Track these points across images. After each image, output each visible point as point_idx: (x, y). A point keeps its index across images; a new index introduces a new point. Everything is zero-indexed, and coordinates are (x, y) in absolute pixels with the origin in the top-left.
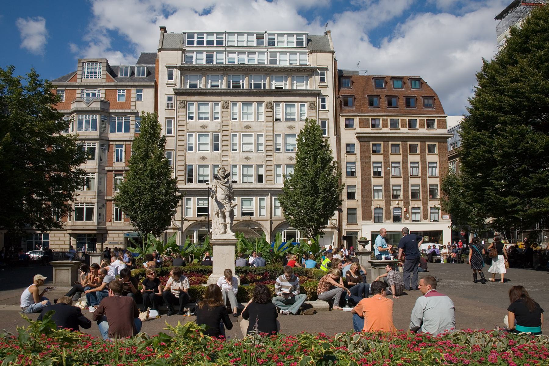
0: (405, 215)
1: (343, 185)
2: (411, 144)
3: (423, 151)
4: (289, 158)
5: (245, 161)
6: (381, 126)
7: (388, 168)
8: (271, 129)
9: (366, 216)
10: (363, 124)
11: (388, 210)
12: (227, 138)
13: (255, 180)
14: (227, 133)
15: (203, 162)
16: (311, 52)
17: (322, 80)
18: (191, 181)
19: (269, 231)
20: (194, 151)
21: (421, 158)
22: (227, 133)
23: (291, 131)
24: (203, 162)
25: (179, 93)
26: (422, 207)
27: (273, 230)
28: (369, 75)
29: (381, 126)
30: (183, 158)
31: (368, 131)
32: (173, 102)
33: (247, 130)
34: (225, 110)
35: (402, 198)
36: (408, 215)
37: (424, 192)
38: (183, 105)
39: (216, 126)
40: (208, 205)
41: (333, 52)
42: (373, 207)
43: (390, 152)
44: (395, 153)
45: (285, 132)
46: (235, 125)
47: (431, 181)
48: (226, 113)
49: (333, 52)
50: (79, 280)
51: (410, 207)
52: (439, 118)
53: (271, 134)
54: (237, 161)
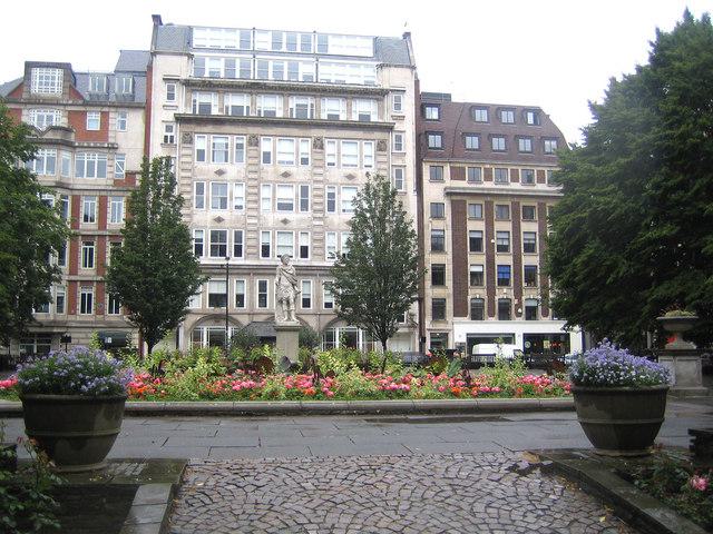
0: (516, 310)
8: (321, 178)
9: (460, 311)
11: (491, 301)
17: (398, 106)
25: (180, 119)
36: (520, 310)
37: (517, 273)
39: (239, 172)
42: (469, 297)
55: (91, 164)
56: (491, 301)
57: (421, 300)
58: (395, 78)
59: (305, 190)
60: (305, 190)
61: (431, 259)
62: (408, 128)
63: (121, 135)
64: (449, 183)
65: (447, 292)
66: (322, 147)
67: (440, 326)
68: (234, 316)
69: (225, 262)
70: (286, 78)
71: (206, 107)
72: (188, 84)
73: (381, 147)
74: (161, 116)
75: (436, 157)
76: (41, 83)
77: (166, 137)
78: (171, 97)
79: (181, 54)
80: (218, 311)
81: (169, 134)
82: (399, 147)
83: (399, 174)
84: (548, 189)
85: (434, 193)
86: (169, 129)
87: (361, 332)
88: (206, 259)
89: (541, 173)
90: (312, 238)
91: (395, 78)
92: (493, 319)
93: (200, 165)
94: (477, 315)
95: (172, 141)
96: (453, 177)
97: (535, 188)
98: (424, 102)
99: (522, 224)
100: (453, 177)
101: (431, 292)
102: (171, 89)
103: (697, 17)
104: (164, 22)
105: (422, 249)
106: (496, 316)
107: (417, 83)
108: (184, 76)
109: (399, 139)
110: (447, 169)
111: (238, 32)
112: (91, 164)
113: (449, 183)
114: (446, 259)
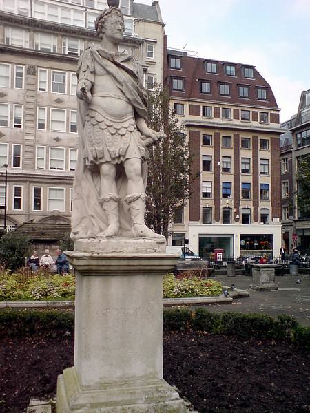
0: (235, 216)
2: (240, 139)
3: (255, 146)
4: (55, 139)
6: (251, 119)
7: (219, 163)
9: (194, 217)
10: (194, 111)
11: (217, 209)
16: (138, 21)
17: (150, 54)
18: (17, 163)
20: (45, 130)
21: (253, 154)
26: (252, 208)
27: (11, 216)
28: (200, 57)
29: (251, 119)
31: (198, 119)
33: (58, 105)
34: (29, 76)
35: (233, 197)
36: (238, 217)
37: (236, 188)
39: (18, 96)
41: (163, 25)
42: (201, 206)
43: (221, 146)
44: (226, 146)
46: (43, 97)
47: (263, 180)
48: (31, 81)
49: (163, 25)
50: (217, 317)
51: (240, 207)
52: (272, 112)
66: (34, 74)
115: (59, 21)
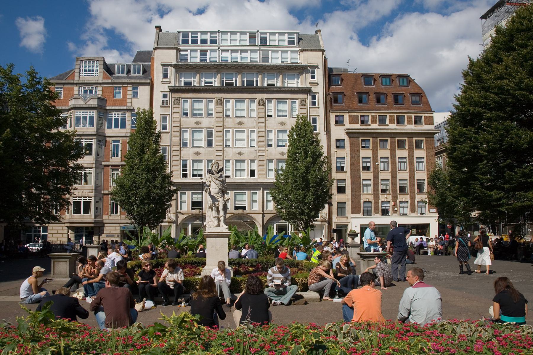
0: (393, 208)
1: (333, 180)
2: (399, 140)
3: (410, 146)
4: (280, 154)
5: (238, 156)
6: (370, 123)
7: (377, 163)
8: (263, 125)
9: (356, 210)
10: (353, 120)
11: (377, 203)
12: (221, 134)
13: (248, 175)
14: (221, 129)
15: (197, 157)
16: (302, 51)
17: (313, 77)
19: (261, 224)
20: (188, 146)
21: (409, 153)
22: (221, 129)
23: (282, 127)
24: (197, 157)
25: (173, 90)
26: (409, 201)
28: (358, 72)
29: (370, 123)
30: (178, 153)
31: (358, 127)
32: (168, 99)
33: (240, 126)
34: (218, 106)
35: (391, 192)
36: (396, 209)
37: (412, 187)
38: (178, 102)
39: (210, 122)
40: (202, 199)
41: (323, 51)
42: (362, 201)
43: (379, 148)
44: (384, 148)
45: (277, 128)
46: (228, 122)
47: (418, 176)
48: (220, 110)
49: (323, 51)
50: (76, 271)
51: (398, 201)
52: (426, 115)
53: (263, 130)
54: (230, 156)
55: (116, 120)
56: (377, 203)
57: (330, 205)
58: (312, 58)
59: (210, 134)
60: (210, 134)
61: (336, 175)
62: (319, 90)
63: (135, 100)
64: (348, 125)
65: (346, 198)
67: (342, 221)
68: (265, 223)
69: (200, 181)
70: (239, 61)
71: (188, 84)
72: (176, 67)
73: (303, 103)
74: (160, 88)
75: (339, 109)
76: (85, 71)
77: (163, 101)
78: (166, 76)
79: (172, 48)
80: (197, 212)
81: (165, 99)
82: (314, 103)
83: (314, 120)
84: (378, 127)
85: (338, 132)
86: (165, 96)
87: (290, 226)
88: (177, 179)
89: (409, 118)
90: (257, 163)
91: (312, 58)
92: (377, 215)
93: (184, 118)
94: (367, 213)
95: (167, 104)
96: (351, 122)
97: (406, 128)
98: (331, 76)
99: (397, 151)
100: (351, 122)
101: (336, 198)
102: (166, 71)
103: (97, 43)
104: (164, 30)
105: (330, 169)
106: (361, 213)
107: (325, 60)
108: (174, 62)
109: (314, 98)
110: (346, 117)
111: (248, 34)
112: (116, 120)
113: (348, 125)
114: (347, 176)
115: (289, 62)
